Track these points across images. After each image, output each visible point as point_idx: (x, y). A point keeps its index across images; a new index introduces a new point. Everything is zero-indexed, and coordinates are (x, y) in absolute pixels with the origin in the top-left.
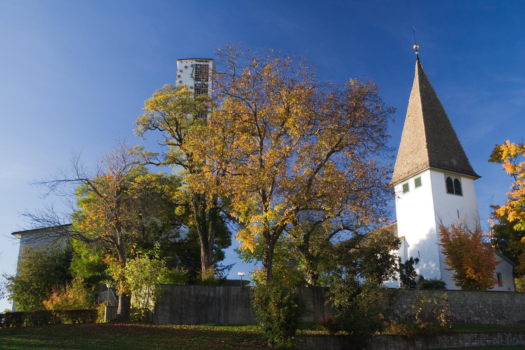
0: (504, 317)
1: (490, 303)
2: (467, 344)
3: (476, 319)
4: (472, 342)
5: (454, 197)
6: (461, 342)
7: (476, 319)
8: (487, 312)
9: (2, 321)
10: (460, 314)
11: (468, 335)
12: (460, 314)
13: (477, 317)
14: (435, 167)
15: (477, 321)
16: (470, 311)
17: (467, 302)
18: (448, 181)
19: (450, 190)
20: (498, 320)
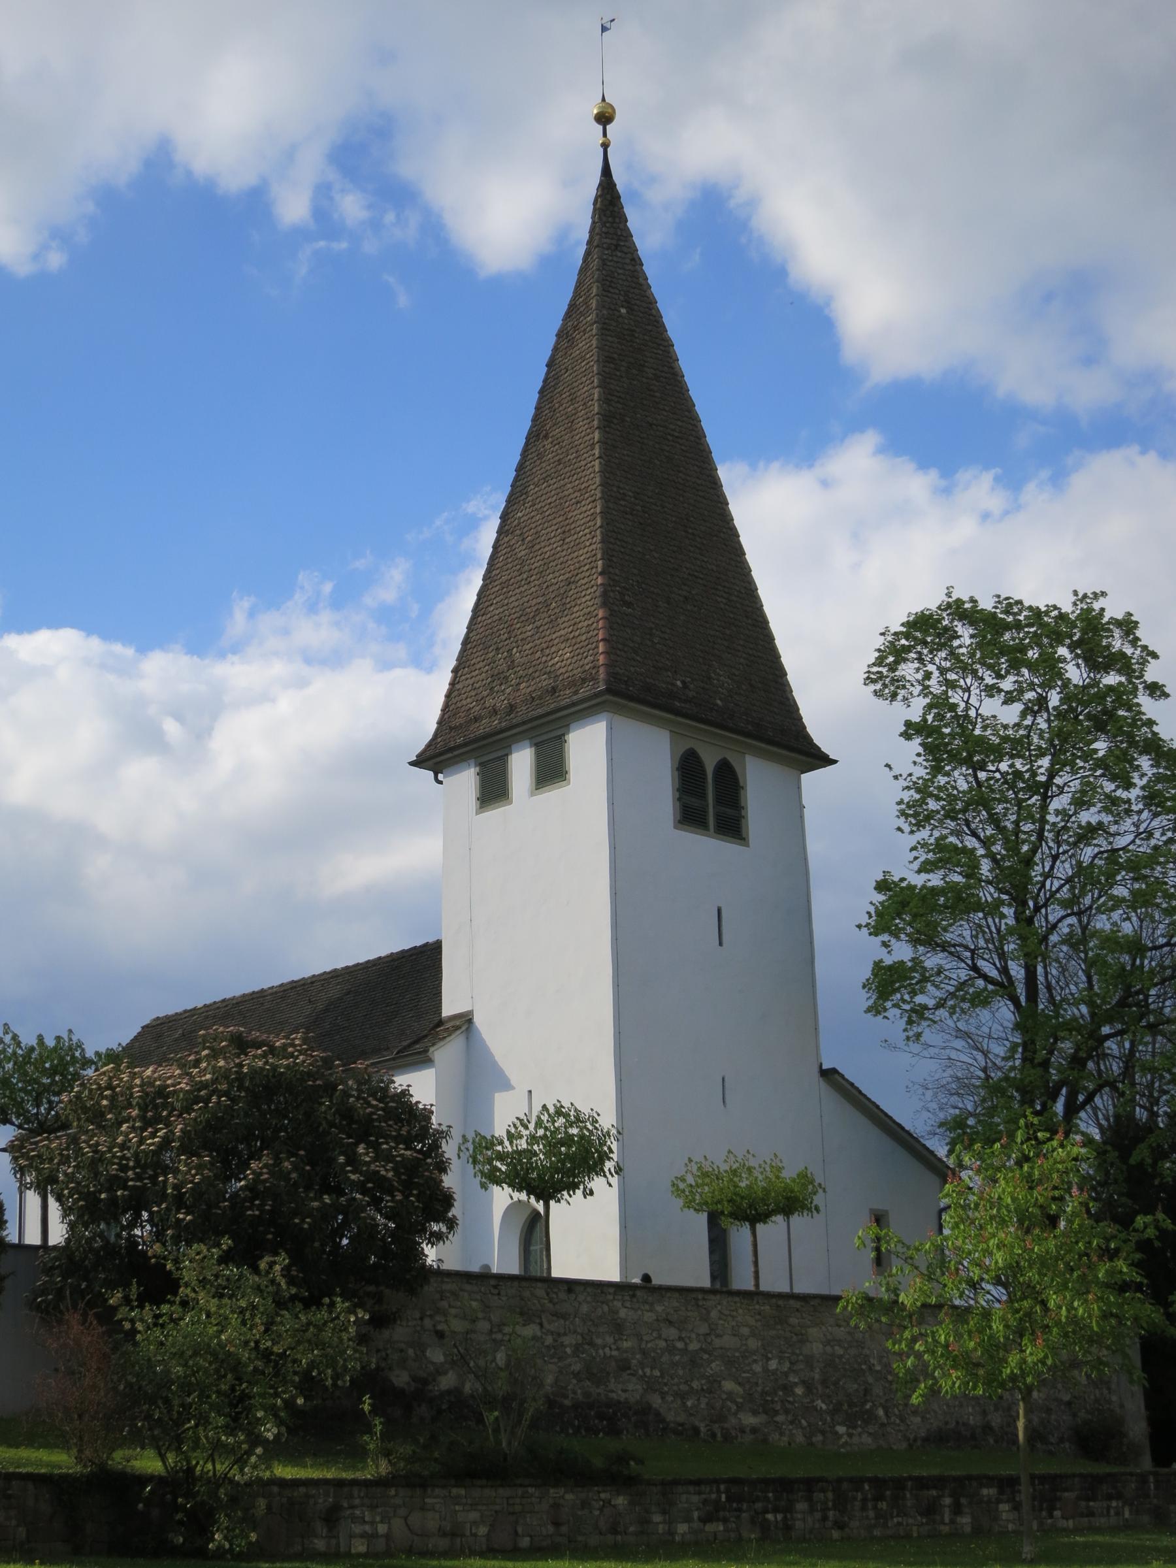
0: (869, 1417)
1: (816, 1348)
2: (682, 1528)
3: (749, 1420)
4: (705, 1520)
5: (705, 847)
6: (657, 1518)
7: (749, 1420)
8: (799, 1391)
9: (309, 1224)
10: (683, 1396)
11: (691, 1489)
12: (683, 1396)
13: (755, 1413)
14: (631, 698)
15: (754, 1430)
16: (728, 1385)
17: (717, 1342)
18: (688, 771)
19: (690, 816)
20: (841, 1429)
